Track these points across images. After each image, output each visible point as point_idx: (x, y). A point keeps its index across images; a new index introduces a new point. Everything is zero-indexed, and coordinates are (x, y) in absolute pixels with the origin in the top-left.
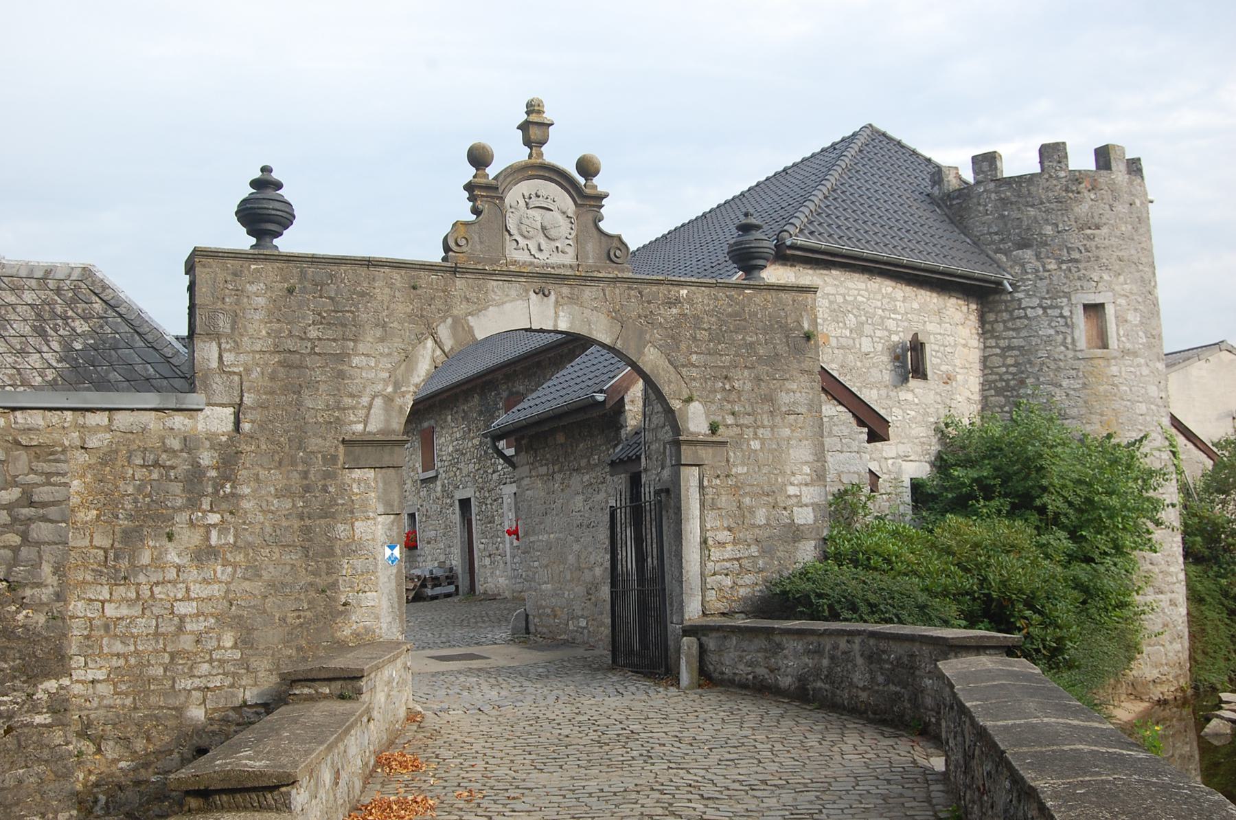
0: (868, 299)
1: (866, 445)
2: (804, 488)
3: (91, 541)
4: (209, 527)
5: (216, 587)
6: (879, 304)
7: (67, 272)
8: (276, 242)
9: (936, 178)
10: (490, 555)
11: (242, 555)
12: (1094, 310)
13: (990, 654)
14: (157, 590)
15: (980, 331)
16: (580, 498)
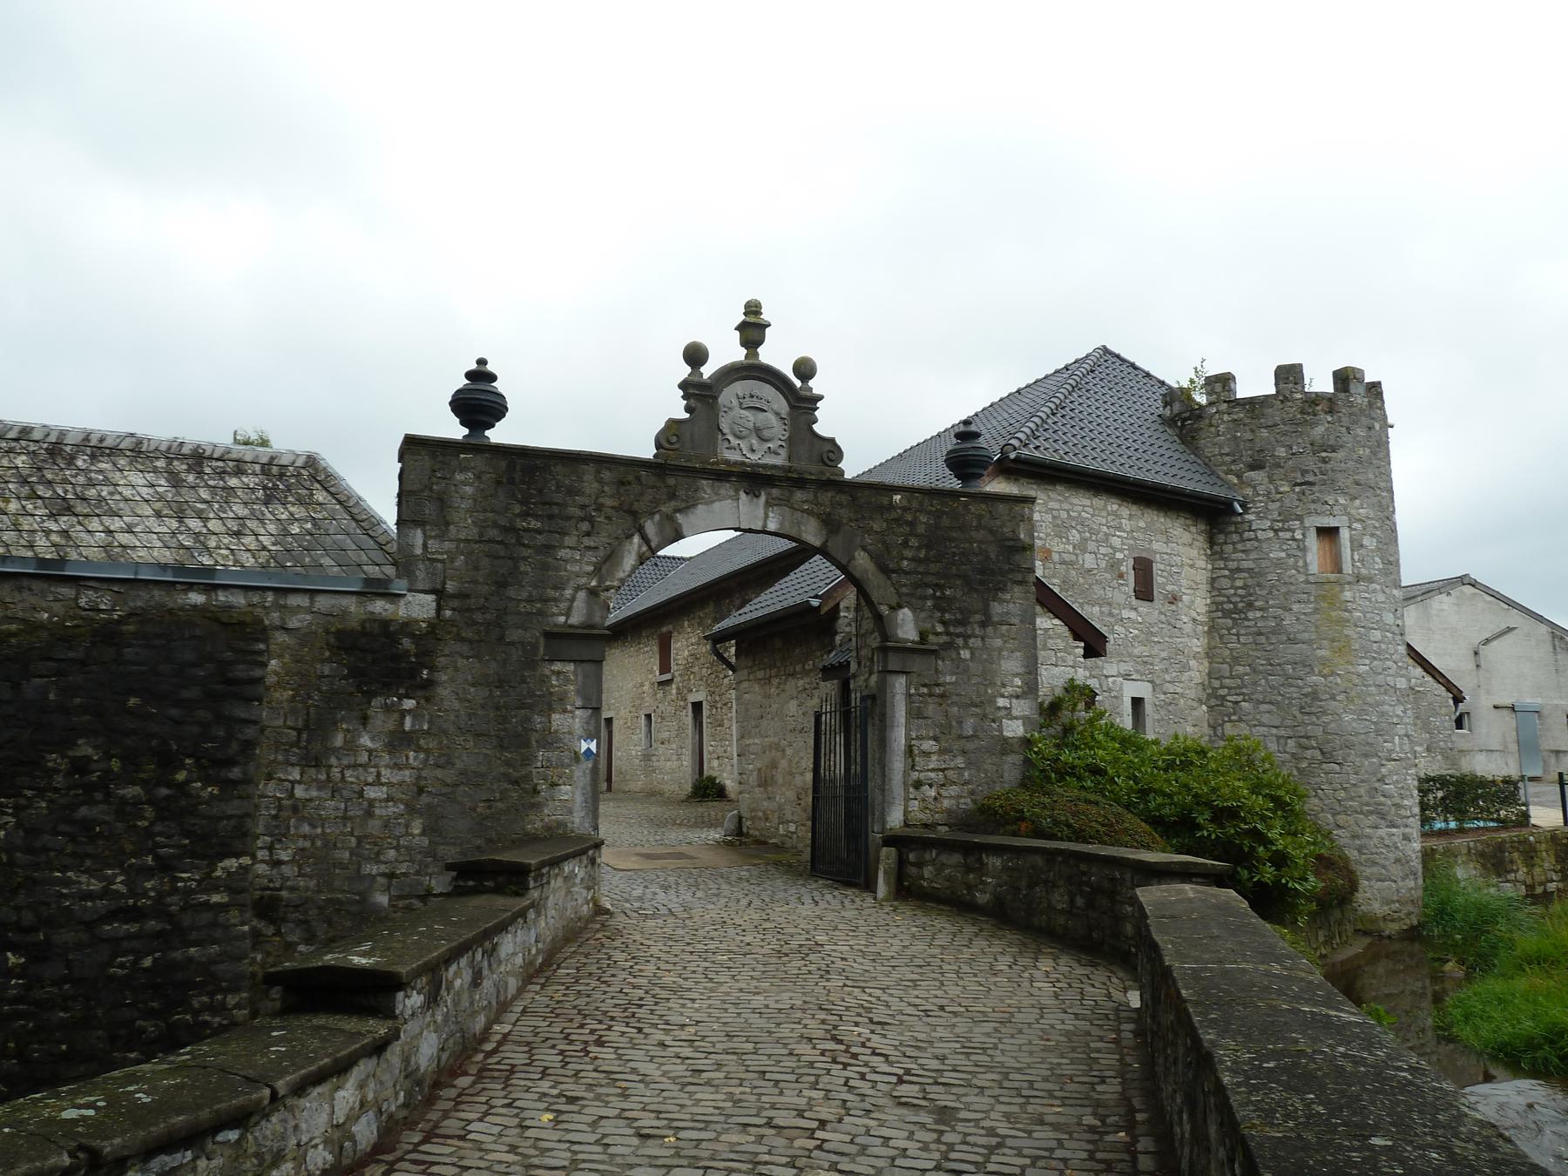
0: (1093, 516)
2: (1014, 701)
3: (285, 722)
4: (403, 713)
5: (407, 772)
6: (1104, 521)
7: (292, 458)
8: (487, 433)
9: (1168, 399)
10: (718, 758)
12: (1329, 533)
13: (1197, 883)
14: (348, 773)
15: (1209, 552)
16: (794, 703)
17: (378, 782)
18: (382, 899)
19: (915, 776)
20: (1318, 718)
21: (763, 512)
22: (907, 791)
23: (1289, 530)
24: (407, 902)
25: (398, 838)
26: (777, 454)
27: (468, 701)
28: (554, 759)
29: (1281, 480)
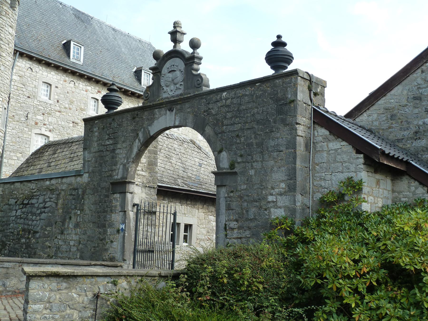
2: (279, 197)
21: (174, 117)
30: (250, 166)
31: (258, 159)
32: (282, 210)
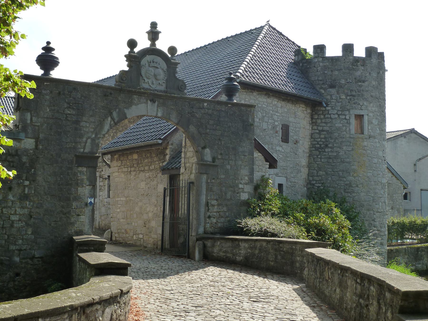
0: (267, 106)
1: (268, 169)
2: (245, 186)
5: (26, 210)
11: (36, 198)
12: (360, 117)
14: (4, 210)
15: (311, 122)
16: (144, 183)
17: (15, 214)
18: (17, 259)
19: (208, 214)
20: (351, 194)
22: (205, 220)
23: (344, 115)
24: (26, 260)
25: (23, 236)
26: (162, 85)
27: (48, 182)
28: (79, 205)
29: (342, 93)
30: (227, 163)
31: (233, 158)
32: (247, 194)
